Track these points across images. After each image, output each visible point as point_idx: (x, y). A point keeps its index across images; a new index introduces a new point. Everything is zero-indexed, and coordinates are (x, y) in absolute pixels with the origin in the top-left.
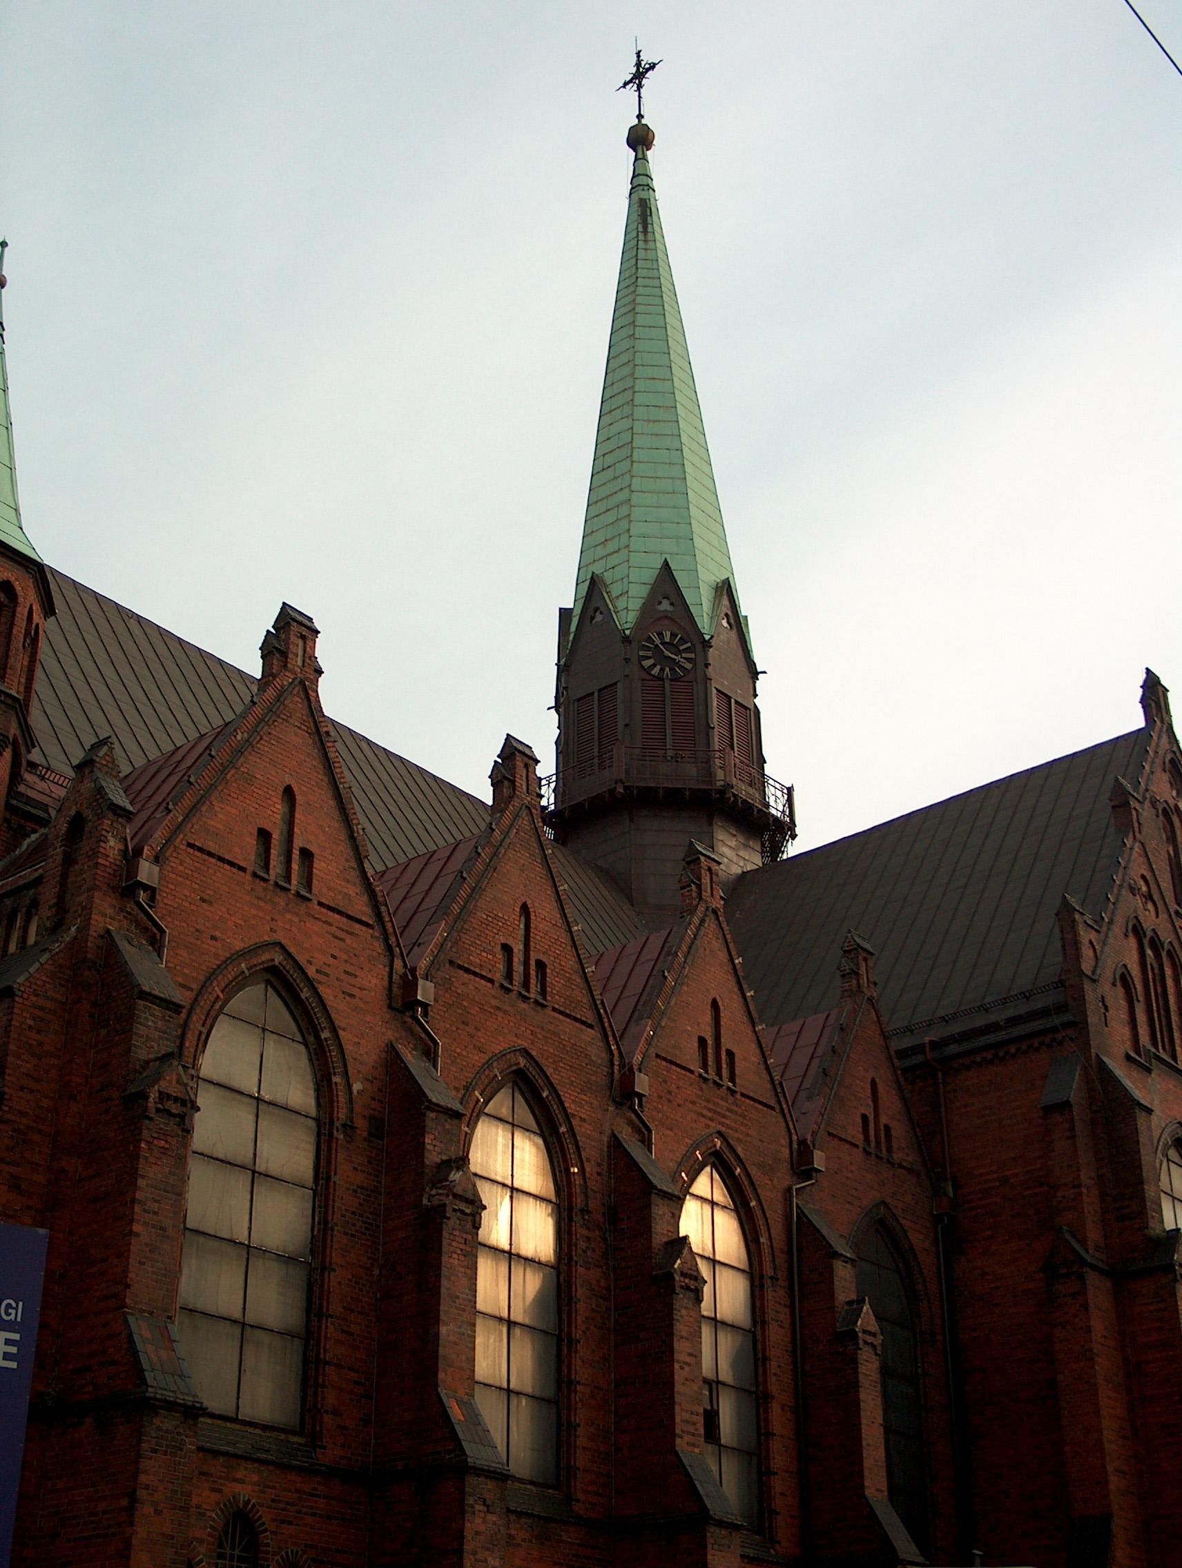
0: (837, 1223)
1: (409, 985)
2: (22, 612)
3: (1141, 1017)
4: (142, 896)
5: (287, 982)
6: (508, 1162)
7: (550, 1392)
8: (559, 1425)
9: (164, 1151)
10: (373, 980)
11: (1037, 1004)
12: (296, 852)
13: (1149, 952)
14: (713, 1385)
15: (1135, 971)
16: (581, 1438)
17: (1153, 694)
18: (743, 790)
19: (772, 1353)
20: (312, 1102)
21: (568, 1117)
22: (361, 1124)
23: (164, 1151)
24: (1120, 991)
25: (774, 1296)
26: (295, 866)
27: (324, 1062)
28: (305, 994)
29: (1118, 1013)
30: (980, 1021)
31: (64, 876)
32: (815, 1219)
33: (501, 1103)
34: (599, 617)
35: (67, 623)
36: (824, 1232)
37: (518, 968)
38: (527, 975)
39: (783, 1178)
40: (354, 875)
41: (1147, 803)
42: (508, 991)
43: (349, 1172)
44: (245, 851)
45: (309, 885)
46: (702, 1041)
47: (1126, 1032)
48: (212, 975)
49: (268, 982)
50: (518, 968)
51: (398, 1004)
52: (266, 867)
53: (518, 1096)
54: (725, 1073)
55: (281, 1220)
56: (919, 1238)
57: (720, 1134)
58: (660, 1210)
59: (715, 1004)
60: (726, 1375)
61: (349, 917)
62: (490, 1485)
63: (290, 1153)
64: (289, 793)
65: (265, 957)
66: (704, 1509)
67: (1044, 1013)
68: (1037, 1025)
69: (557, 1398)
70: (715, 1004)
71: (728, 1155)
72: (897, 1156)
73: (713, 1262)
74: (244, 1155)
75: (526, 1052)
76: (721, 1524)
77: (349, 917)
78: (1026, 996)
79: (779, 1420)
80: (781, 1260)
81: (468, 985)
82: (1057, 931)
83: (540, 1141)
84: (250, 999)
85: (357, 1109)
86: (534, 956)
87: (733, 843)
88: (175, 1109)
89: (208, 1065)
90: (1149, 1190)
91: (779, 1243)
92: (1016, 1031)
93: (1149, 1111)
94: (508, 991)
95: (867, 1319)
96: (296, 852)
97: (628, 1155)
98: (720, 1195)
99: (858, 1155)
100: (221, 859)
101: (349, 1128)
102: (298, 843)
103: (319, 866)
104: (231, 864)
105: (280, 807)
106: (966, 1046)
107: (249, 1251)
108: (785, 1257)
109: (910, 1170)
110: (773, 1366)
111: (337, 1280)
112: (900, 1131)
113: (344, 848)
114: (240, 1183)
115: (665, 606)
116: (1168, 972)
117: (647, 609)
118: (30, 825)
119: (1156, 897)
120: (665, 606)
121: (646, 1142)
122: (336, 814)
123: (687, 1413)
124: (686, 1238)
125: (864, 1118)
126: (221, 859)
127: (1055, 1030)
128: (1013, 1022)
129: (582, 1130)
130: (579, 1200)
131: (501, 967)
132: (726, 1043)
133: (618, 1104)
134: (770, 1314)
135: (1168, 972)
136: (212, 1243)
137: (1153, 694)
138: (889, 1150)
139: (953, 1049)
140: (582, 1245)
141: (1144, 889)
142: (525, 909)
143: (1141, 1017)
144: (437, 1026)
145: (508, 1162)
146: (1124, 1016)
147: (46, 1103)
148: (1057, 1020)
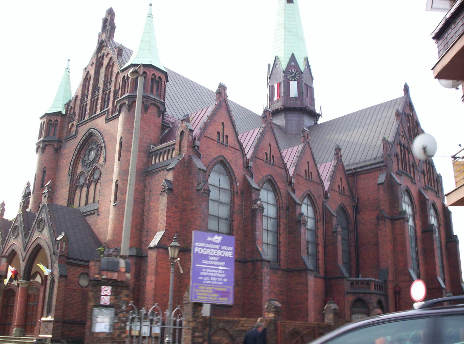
0: (333, 208)
1: (248, 163)
2: (163, 83)
3: (400, 163)
4: (196, 148)
5: (224, 163)
6: (266, 196)
7: (275, 244)
8: (278, 250)
9: (205, 200)
10: (240, 162)
11: (377, 161)
12: (225, 136)
13: (402, 148)
14: (308, 242)
15: (399, 153)
16: (282, 253)
17: (406, 89)
18: (310, 107)
19: (319, 235)
20: (230, 188)
21: (279, 188)
22: (239, 192)
23: (205, 200)
24: (396, 158)
25: (320, 224)
26: (225, 139)
27: (232, 180)
28: (228, 166)
29: (395, 163)
30: (364, 164)
31: (180, 143)
32: (329, 208)
33: (266, 186)
34: (277, 66)
35: (171, 83)
36: (331, 210)
37: (269, 157)
38: (270, 159)
39: (322, 199)
40: (236, 140)
41: (403, 114)
42: (267, 162)
43: (237, 201)
44: (215, 137)
45: (228, 143)
46: (305, 171)
47: (397, 167)
48: (210, 163)
49: (221, 164)
50: (269, 157)
51: (245, 166)
52: (219, 140)
53: (269, 185)
54: (310, 177)
55: (224, 212)
56: (350, 211)
57: (309, 190)
58: (298, 207)
59: (308, 162)
60: (310, 240)
61: (235, 149)
62: (267, 263)
63: (225, 198)
64: (223, 123)
65: (220, 158)
66: (307, 267)
67: (378, 163)
68: (377, 166)
69: (277, 246)
70: (308, 162)
71: (311, 195)
72: (346, 193)
73: (308, 217)
74: (217, 199)
75: (270, 175)
76: (310, 270)
77: (235, 149)
78: (375, 159)
79: (321, 249)
80: (321, 216)
81: (259, 162)
82: (382, 144)
83: (273, 194)
84: (218, 167)
85: (239, 189)
86: (271, 155)
87: (307, 119)
88: (207, 192)
89: (210, 181)
90: (400, 201)
91: (321, 212)
92: (373, 167)
93: (401, 185)
94: (267, 162)
95: (339, 229)
96: (225, 136)
97: (291, 196)
98: (309, 203)
99: (337, 194)
100: (211, 139)
101: (237, 192)
102: (225, 134)
103: (229, 139)
104: (212, 139)
105: (221, 127)
106: (361, 170)
107: (219, 218)
108: (323, 216)
109: (348, 196)
110: (320, 238)
111: (236, 223)
112: (346, 188)
113: (234, 134)
114: (217, 204)
115: (293, 63)
116: (406, 152)
117: (289, 65)
118: (166, 128)
119: (405, 136)
120: (293, 63)
121: (294, 193)
122: (232, 127)
123: (303, 248)
124: (303, 213)
125: (339, 186)
126: (211, 139)
127: (381, 167)
128: (371, 165)
129: (282, 191)
130: (281, 205)
131: (265, 158)
132: (310, 171)
133: (288, 185)
134: (319, 227)
135: (406, 152)
136: (212, 217)
137: (406, 89)
138: (344, 192)
139: (359, 170)
140: (282, 214)
141: (402, 134)
142: (270, 144)
143: (400, 163)
144: (253, 171)
145: (266, 196)
146: (396, 163)
147: (180, 190)
148: (381, 165)
